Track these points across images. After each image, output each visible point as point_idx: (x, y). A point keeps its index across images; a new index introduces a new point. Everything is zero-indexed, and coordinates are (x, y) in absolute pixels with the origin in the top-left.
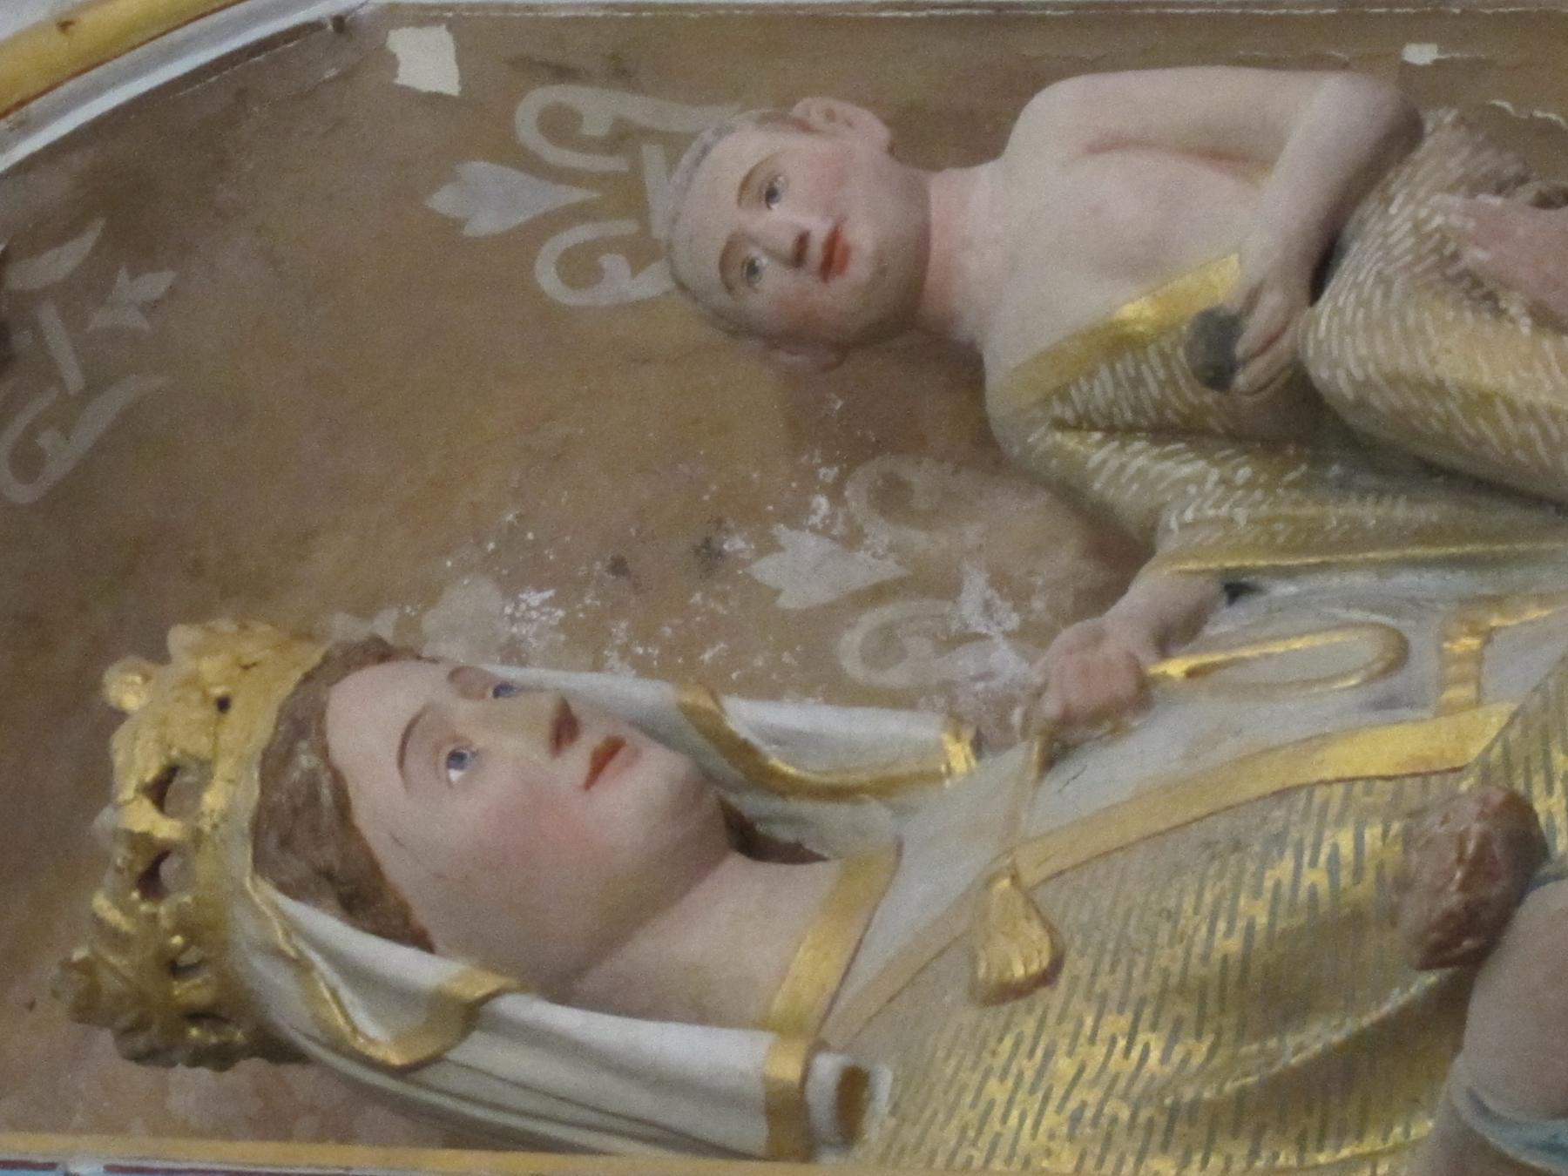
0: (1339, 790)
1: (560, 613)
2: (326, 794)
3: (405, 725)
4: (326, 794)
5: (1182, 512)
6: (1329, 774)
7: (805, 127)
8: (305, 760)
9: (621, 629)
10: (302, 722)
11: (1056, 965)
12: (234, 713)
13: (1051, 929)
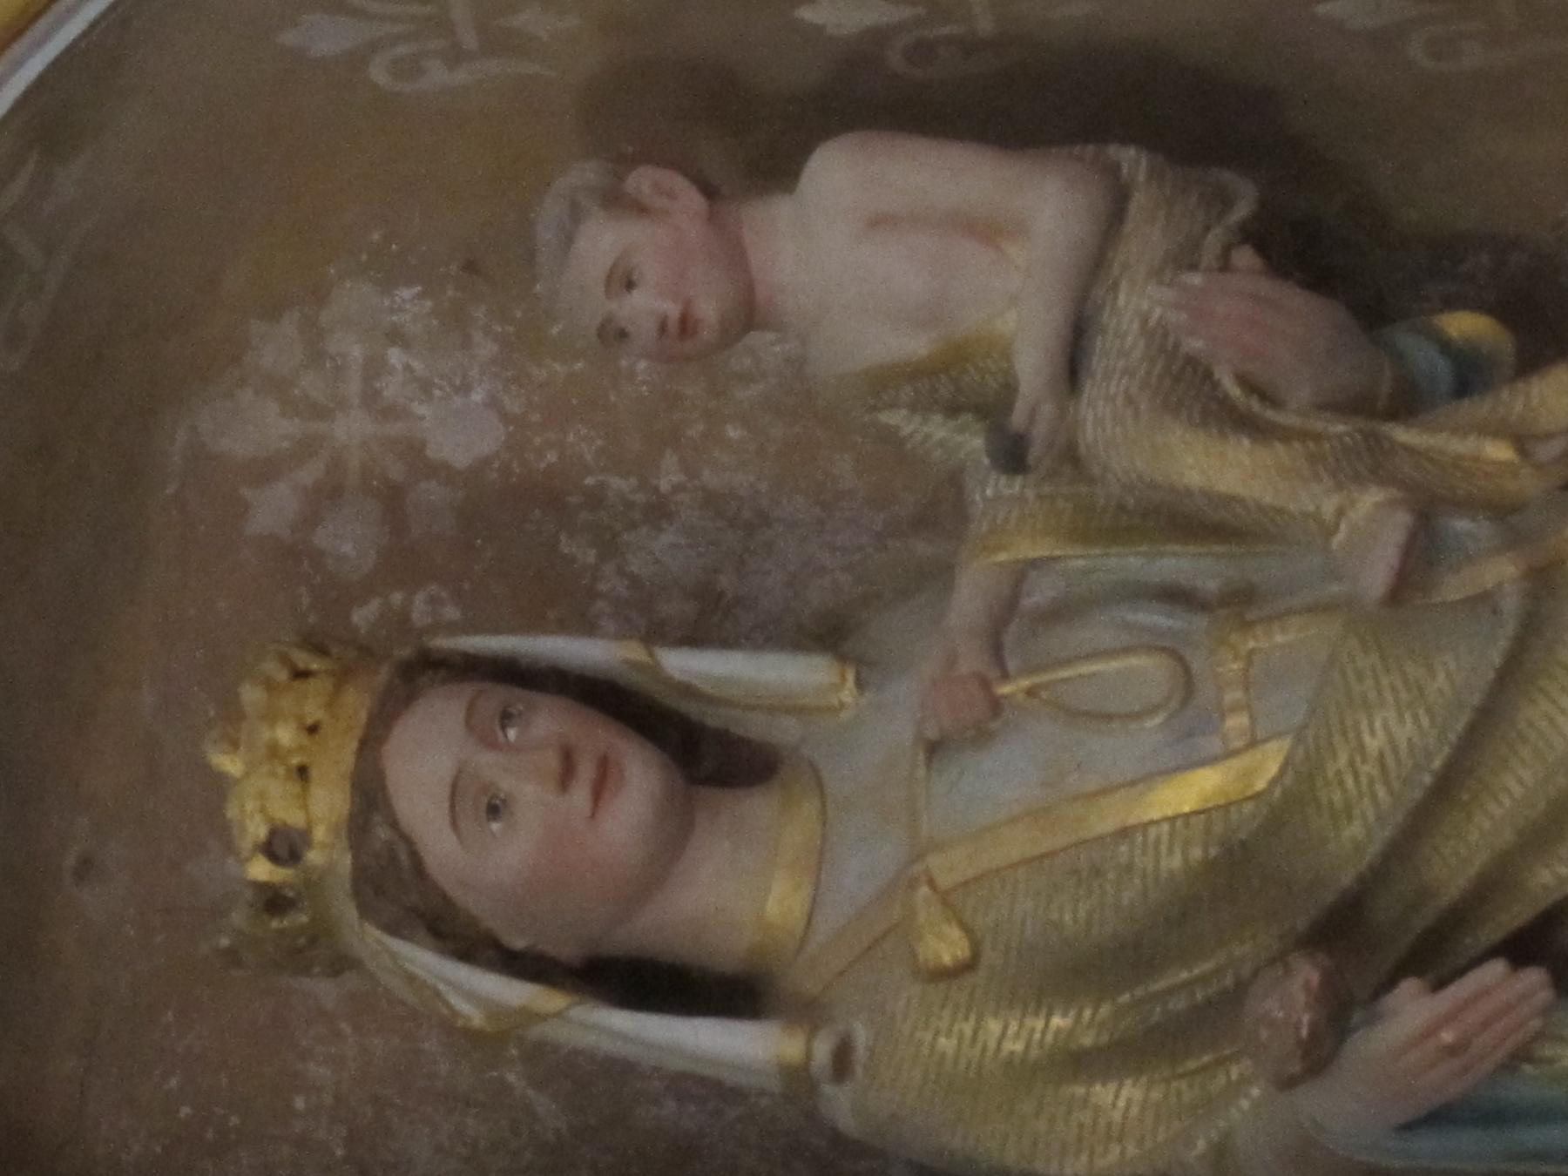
0: (1166, 827)
1: (429, 304)
2: (403, 857)
3: (449, 780)
4: (403, 857)
5: (984, 491)
6: (1155, 814)
7: (641, 209)
8: (383, 833)
9: (480, 313)
10: (370, 795)
11: (976, 956)
12: (314, 773)
13: (967, 929)
